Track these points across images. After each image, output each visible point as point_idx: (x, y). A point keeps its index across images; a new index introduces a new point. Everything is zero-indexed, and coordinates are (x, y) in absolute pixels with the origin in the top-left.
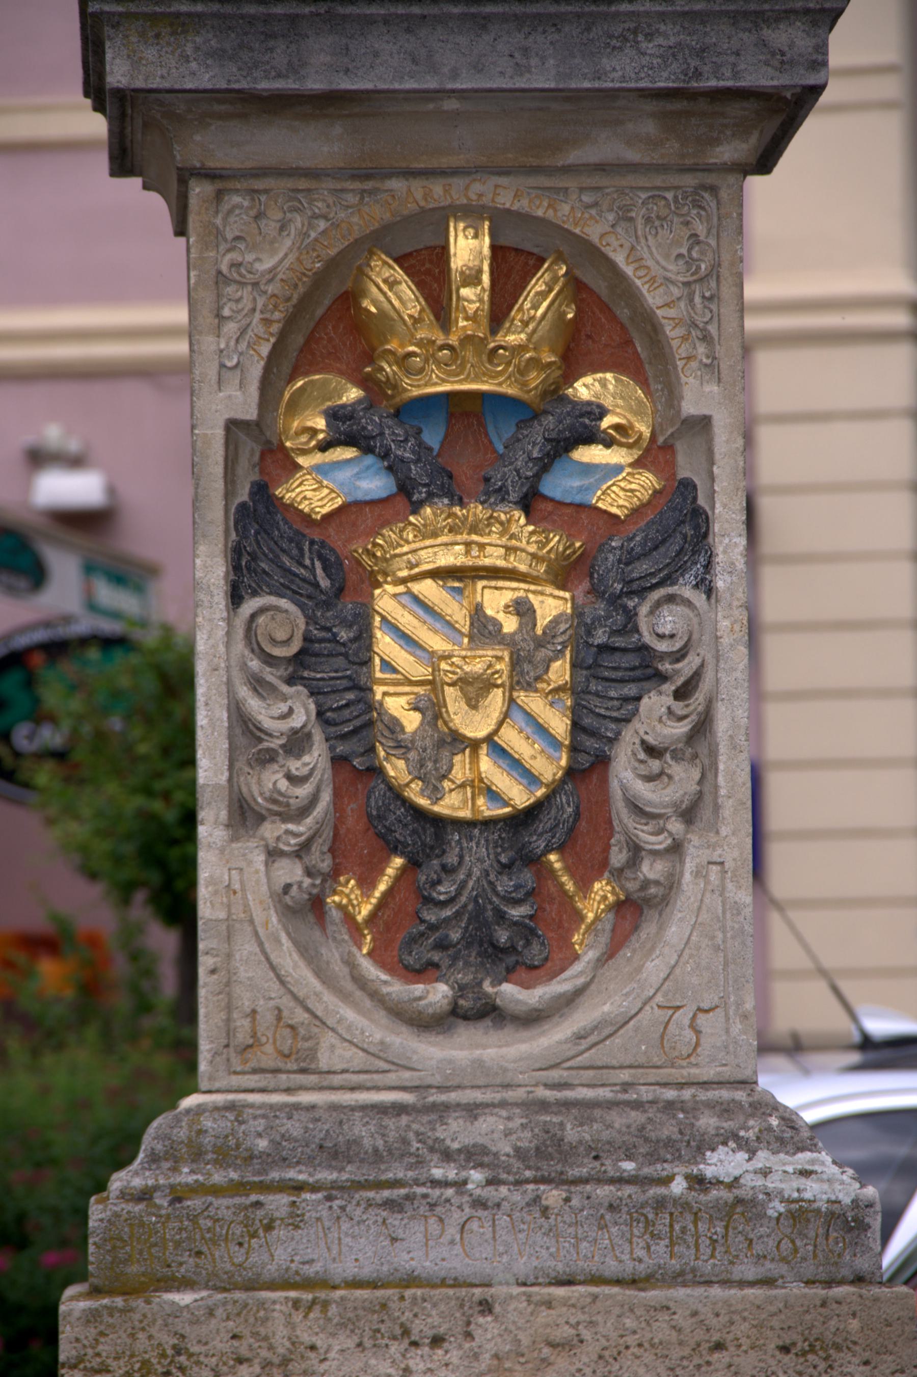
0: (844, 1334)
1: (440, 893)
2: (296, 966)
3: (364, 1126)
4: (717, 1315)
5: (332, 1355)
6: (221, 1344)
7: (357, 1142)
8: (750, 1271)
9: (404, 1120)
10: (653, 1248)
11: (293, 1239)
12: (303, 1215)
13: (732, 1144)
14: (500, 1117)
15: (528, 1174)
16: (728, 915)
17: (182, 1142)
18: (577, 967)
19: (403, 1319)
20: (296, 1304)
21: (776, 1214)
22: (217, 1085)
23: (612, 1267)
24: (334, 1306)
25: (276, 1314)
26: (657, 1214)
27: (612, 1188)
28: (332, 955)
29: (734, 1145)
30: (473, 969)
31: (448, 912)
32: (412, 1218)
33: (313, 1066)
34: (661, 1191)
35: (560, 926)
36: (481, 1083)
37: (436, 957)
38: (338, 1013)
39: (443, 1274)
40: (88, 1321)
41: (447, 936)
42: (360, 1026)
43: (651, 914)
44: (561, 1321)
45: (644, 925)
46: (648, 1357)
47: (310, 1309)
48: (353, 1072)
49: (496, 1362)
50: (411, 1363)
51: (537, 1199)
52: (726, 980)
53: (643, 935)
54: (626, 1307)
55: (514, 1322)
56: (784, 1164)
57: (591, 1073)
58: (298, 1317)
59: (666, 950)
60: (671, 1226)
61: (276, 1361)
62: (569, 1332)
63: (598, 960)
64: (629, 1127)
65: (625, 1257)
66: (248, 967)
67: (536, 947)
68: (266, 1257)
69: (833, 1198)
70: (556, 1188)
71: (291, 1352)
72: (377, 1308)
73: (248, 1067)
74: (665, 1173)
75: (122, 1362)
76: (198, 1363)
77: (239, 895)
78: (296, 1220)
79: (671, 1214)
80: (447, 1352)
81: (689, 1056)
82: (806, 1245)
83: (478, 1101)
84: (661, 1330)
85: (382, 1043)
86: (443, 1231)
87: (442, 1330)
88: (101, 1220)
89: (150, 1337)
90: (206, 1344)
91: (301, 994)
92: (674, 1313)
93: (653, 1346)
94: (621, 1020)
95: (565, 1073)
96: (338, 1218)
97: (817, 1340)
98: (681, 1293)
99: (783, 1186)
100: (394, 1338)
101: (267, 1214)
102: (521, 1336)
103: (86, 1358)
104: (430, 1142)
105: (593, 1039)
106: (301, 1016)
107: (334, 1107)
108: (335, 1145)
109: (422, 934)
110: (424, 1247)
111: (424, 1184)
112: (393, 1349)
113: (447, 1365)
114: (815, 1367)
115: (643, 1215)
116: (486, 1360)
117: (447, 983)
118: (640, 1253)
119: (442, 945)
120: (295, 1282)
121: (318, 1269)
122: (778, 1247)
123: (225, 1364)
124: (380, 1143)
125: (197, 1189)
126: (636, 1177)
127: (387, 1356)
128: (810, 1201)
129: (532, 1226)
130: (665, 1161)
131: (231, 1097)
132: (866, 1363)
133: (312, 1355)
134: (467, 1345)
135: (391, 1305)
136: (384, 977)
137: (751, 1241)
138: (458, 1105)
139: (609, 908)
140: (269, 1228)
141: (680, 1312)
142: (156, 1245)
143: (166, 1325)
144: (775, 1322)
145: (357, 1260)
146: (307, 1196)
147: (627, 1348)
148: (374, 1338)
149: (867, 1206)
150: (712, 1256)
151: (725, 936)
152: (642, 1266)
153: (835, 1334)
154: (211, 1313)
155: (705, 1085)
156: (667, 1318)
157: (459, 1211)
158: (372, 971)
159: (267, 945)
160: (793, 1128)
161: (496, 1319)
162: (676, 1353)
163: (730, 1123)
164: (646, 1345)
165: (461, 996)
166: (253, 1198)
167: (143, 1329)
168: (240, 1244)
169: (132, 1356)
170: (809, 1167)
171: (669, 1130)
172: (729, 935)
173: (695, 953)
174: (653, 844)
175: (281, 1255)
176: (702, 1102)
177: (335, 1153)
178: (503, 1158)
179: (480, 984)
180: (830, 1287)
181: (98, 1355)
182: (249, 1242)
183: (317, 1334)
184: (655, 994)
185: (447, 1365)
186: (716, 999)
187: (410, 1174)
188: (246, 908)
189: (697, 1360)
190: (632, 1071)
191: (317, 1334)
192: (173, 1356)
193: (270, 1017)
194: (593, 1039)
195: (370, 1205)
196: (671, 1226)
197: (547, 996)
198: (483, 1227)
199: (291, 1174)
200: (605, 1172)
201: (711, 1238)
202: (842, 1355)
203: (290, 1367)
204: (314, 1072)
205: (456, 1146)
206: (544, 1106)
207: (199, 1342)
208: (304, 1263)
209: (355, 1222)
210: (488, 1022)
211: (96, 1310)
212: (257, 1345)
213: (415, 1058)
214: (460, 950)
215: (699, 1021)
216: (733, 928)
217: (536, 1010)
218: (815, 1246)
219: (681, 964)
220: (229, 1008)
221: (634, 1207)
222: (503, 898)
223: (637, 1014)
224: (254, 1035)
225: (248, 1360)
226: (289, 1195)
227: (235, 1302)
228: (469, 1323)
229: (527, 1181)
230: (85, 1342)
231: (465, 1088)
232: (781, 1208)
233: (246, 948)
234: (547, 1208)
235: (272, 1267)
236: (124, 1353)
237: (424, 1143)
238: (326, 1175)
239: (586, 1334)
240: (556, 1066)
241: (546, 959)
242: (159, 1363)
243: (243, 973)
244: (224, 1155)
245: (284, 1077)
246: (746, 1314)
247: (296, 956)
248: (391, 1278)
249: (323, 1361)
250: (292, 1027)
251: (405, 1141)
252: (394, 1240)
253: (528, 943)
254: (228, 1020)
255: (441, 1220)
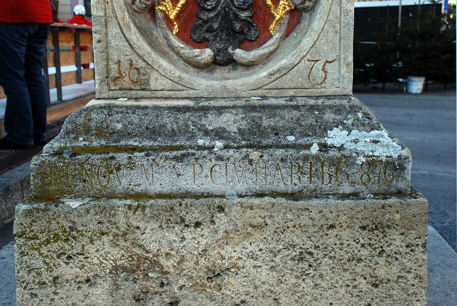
0: (392, 221)
1: (208, 6)
2: (138, 40)
3: (168, 118)
4: (332, 212)
5: (147, 231)
6: (93, 226)
7: (164, 126)
8: (347, 189)
9: (188, 114)
10: (301, 179)
11: (130, 174)
12: (135, 163)
13: (341, 127)
14: (232, 113)
15: (244, 143)
16: (342, 16)
17: (81, 125)
18: (271, 42)
19: (181, 214)
20: (130, 207)
21: (361, 163)
22: (103, 96)
23: (282, 187)
24: (148, 208)
25: (119, 212)
26: (304, 163)
27: (283, 150)
28: (158, 34)
29: (341, 128)
30: (224, 42)
31: (212, 15)
32: (187, 165)
33: (148, 88)
34: (307, 152)
35: (264, 22)
36: (226, 96)
37: (207, 36)
38: (159, 63)
39: (202, 191)
40: (26, 215)
41: (212, 26)
42: (169, 69)
43: (306, 15)
44: (257, 215)
45: (302, 21)
46: (298, 232)
47: (136, 209)
48: (166, 90)
49: (226, 234)
50: (185, 235)
51: (247, 156)
52: (340, 48)
53: (302, 26)
54: (288, 209)
55: (234, 216)
56: (365, 137)
57: (276, 91)
58: (130, 214)
59: (312, 33)
60: (311, 168)
61: (120, 234)
62: (260, 220)
63: (281, 38)
64: (292, 119)
65: (289, 183)
66: (117, 42)
67: (253, 31)
68: (117, 183)
69: (389, 155)
70: (256, 150)
71: (127, 230)
72: (169, 209)
73: (117, 88)
74: (308, 142)
75: (44, 235)
76: (82, 235)
77: (110, 4)
78: (131, 165)
79: (311, 163)
80: (202, 230)
81: (321, 83)
82: (375, 177)
83: (223, 105)
84: (305, 219)
85: (180, 77)
86: (202, 171)
87: (200, 220)
88: (36, 165)
89: (58, 223)
90: (86, 226)
91: (141, 54)
92: (311, 212)
93: (300, 227)
94: (290, 66)
95: (264, 91)
96: (152, 165)
97: (379, 224)
98: (315, 202)
99: (364, 149)
100: (177, 223)
101: (117, 163)
102: (238, 222)
103: (26, 233)
104: (199, 126)
105: (277, 76)
106: (141, 64)
107: (156, 108)
108: (154, 127)
109: (200, 25)
110: (192, 178)
111: (193, 148)
112: (176, 229)
113: (202, 236)
114: (377, 236)
115: (297, 163)
116: (221, 233)
117: (211, 49)
118: (296, 181)
119: (210, 30)
120: (132, 194)
121: (143, 188)
122: (361, 178)
123: (95, 235)
124: (175, 127)
125: (86, 150)
126: (295, 144)
127: (174, 232)
128: (377, 156)
129: (244, 169)
130: (309, 136)
131: (108, 102)
132: (402, 234)
133: (138, 231)
134: (212, 226)
135: (175, 208)
136: (182, 45)
137: (348, 175)
138: (214, 107)
139: (287, 13)
140: (118, 169)
141: (314, 211)
142: (63, 176)
143: (66, 217)
144: (359, 216)
145: (161, 184)
146: (136, 154)
147: (288, 228)
148: (167, 223)
149: (405, 159)
150: (330, 182)
151: (340, 26)
152: (297, 187)
153: (388, 221)
154: (88, 211)
155: (328, 97)
156: (307, 214)
157: (210, 162)
158: (177, 43)
159: (124, 29)
160: (369, 118)
161: (226, 215)
162: (311, 230)
163: (340, 116)
164: (297, 226)
165: (217, 55)
166: (111, 155)
167: (54, 219)
168: (105, 177)
169: (49, 231)
170: (376, 139)
171: (311, 120)
172: (342, 25)
173: (326, 34)
174: (43, 19)
175: (125, 182)
176: (327, 105)
177: (153, 132)
178: (233, 134)
179: (227, 49)
180: (386, 198)
181: (32, 231)
182: (109, 176)
183: (140, 221)
184: (306, 54)
185: (202, 236)
186: (335, 56)
187: (188, 143)
188: (114, 11)
189: (321, 233)
190: (295, 90)
191: (140, 221)
192: (70, 232)
193: (127, 65)
194: (277, 76)
195: (167, 159)
196: (311, 168)
197: (257, 55)
198: (221, 169)
199: (131, 142)
200: (280, 142)
201: (329, 174)
202: (391, 230)
203: (127, 236)
204: (148, 90)
205: (211, 128)
206: (253, 108)
207: (82, 225)
208: (136, 186)
209: (160, 167)
210: (230, 67)
211: (30, 210)
212: (111, 226)
213: (195, 84)
214: (218, 33)
215: (326, 67)
216: (344, 22)
217: (252, 62)
218: (379, 177)
219: (319, 40)
220: (108, 59)
221: (293, 160)
222: (238, 8)
223: (298, 64)
224: (120, 73)
225: (107, 233)
226: (128, 153)
227: (99, 206)
228: (213, 216)
229: (243, 147)
230: (25, 225)
231: (218, 98)
232: (364, 160)
233: (114, 30)
234: (252, 160)
235: (120, 188)
236: (45, 230)
237: (196, 127)
238: (148, 143)
239: (269, 221)
240: (260, 88)
241: (258, 37)
242: (63, 235)
243: (113, 43)
244: (100, 133)
245: (134, 92)
246: (345, 212)
247: (138, 35)
248: (178, 193)
249: (142, 234)
250: (137, 69)
251: (187, 126)
252: (179, 175)
253: (249, 30)
254: (107, 65)
255: (201, 166)
